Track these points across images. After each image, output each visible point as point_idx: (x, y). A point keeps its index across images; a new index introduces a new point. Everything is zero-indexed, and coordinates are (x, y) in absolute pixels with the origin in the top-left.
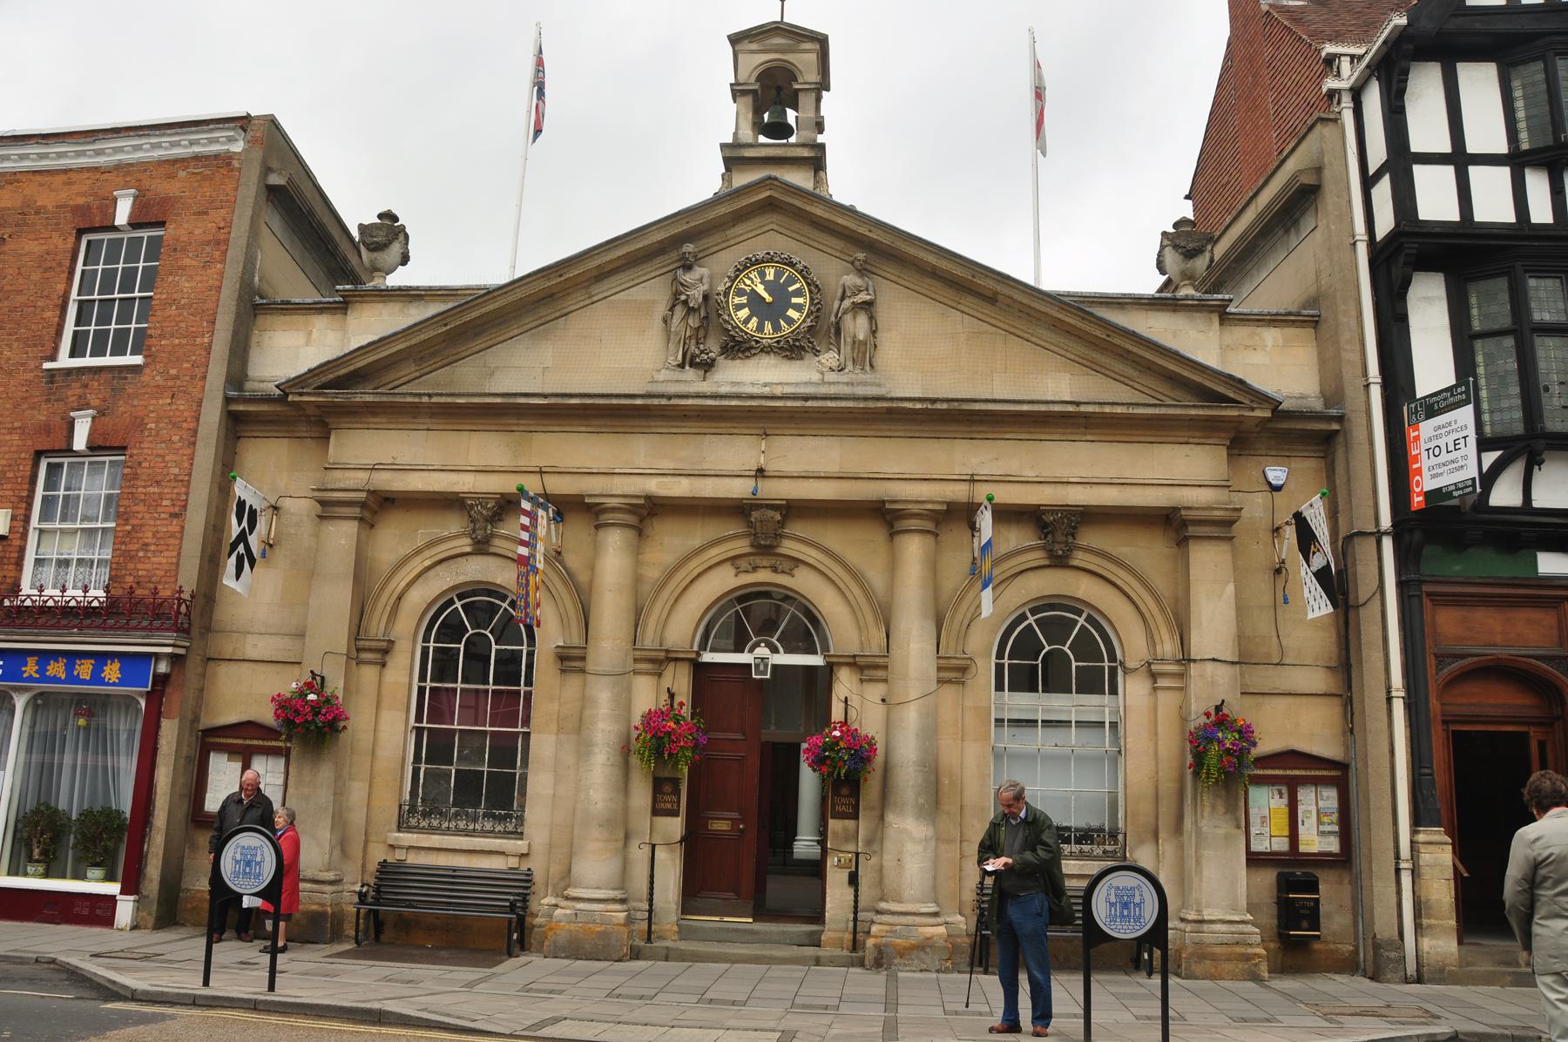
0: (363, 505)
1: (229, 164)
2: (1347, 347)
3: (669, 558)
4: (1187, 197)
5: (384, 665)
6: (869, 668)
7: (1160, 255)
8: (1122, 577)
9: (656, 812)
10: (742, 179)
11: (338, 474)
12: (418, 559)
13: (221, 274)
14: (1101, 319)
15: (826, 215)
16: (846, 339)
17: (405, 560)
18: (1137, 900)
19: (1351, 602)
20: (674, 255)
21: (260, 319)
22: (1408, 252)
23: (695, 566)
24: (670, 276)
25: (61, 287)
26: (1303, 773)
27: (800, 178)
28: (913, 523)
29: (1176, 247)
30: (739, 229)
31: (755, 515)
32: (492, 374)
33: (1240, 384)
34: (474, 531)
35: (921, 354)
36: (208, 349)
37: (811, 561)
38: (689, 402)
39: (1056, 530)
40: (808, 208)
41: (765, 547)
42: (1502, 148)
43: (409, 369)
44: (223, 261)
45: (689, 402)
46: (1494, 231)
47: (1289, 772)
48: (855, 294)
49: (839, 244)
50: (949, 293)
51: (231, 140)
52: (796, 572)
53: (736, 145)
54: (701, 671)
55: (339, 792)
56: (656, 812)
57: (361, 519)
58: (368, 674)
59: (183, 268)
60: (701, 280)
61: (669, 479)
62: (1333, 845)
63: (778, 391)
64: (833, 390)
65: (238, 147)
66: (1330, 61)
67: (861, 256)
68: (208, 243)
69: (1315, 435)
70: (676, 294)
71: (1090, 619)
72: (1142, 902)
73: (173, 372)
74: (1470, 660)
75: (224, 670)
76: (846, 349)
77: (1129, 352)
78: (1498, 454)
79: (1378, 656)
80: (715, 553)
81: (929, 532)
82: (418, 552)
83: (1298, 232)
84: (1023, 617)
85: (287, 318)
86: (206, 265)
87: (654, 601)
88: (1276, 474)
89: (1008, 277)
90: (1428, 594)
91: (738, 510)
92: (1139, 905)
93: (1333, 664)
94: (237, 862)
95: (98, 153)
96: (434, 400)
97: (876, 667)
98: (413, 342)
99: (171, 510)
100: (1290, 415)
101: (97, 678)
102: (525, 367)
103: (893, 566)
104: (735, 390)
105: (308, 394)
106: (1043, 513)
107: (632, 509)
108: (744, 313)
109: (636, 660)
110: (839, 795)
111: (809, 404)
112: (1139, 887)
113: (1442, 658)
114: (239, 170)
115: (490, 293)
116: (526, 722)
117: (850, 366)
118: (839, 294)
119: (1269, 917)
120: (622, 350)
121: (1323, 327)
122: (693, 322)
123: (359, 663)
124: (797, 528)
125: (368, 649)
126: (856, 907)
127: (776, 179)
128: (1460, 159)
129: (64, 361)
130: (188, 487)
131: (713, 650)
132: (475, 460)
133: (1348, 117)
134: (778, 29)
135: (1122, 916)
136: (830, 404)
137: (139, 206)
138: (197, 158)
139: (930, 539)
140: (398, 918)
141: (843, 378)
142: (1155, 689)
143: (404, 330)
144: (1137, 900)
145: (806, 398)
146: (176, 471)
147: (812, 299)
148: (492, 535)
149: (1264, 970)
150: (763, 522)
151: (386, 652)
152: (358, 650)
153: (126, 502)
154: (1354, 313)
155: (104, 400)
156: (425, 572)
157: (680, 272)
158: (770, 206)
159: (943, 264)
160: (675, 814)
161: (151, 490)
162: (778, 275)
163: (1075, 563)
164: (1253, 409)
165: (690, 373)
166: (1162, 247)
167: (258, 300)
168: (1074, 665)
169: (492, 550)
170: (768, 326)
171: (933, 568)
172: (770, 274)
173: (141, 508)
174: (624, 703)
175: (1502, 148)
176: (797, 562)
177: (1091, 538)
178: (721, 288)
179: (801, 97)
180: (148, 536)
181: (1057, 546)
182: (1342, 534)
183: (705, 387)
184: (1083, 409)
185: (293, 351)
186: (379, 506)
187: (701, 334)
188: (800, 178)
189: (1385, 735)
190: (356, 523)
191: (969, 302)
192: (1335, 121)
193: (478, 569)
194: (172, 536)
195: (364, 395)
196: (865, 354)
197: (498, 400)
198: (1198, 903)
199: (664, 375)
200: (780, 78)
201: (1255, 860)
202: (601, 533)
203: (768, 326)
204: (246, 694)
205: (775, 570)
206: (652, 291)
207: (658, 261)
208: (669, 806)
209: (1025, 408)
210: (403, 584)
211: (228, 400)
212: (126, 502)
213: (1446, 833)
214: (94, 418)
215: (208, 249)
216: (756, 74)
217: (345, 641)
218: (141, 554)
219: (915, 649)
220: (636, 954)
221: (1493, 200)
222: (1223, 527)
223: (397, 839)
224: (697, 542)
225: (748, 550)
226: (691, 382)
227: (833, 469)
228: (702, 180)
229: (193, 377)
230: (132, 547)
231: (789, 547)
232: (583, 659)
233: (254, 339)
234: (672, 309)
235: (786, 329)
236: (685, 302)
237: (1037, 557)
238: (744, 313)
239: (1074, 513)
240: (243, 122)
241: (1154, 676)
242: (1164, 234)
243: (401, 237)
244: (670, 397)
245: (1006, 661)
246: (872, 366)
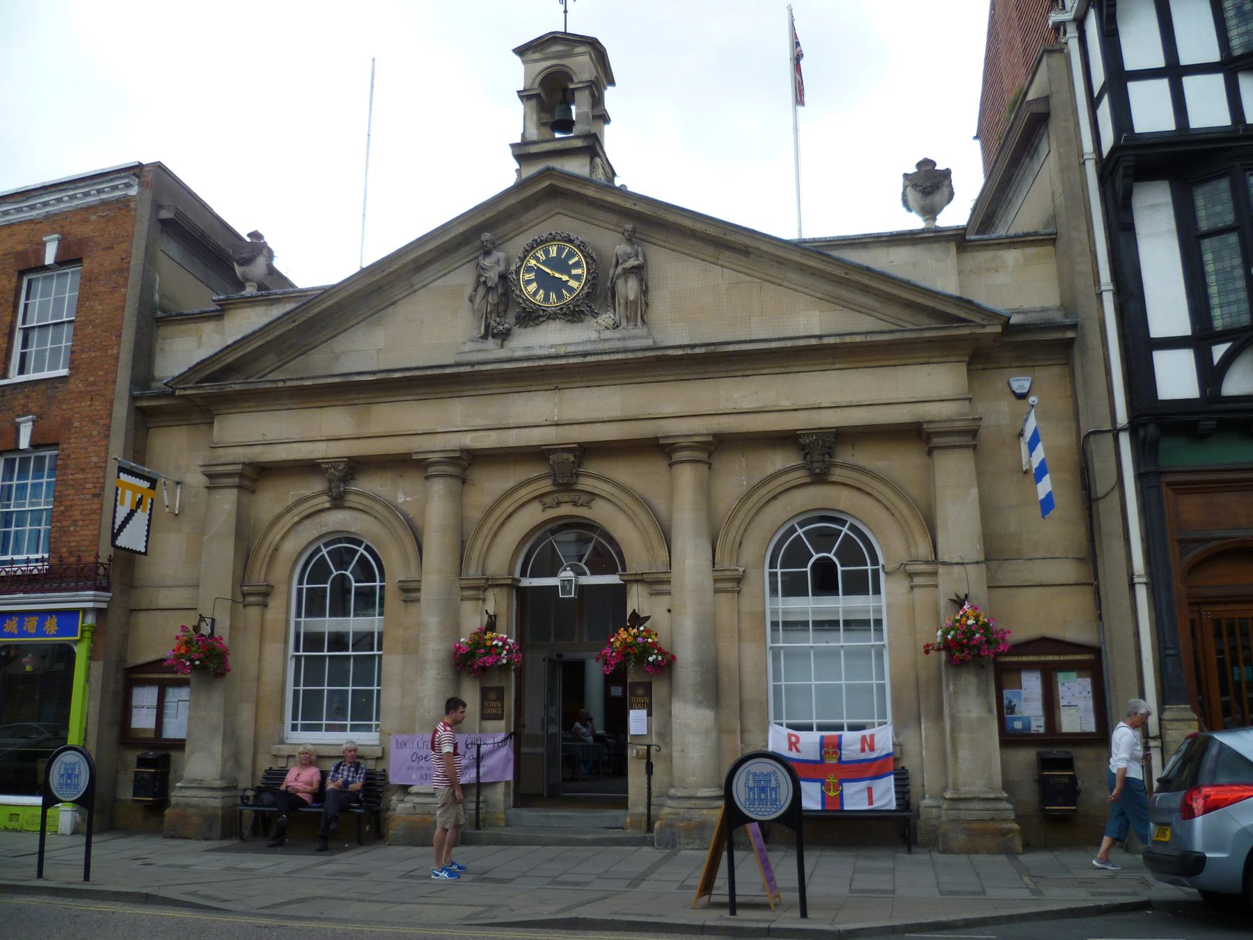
0: (241, 475)
1: (128, 206)
3: (488, 500)
4: (976, 138)
5: (265, 606)
6: (658, 583)
7: (904, 195)
9: (485, 717)
11: (221, 451)
12: (289, 516)
13: (124, 296)
14: (838, 260)
16: (620, 299)
17: (278, 518)
18: (773, 784)
19: (1093, 497)
20: (477, 243)
22: (1137, 162)
23: (508, 506)
24: (473, 264)
25: (8, 319)
26: (1056, 658)
27: (577, 166)
28: (685, 455)
29: (915, 186)
30: (530, 215)
31: (553, 458)
34: (330, 489)
35: (690, 308)
36: (116, 358)
37: (604, 494)
38: (489, 367)
39: (819, 450)
41: (565, 484)
42: (1214, 55)
43: (271, 360)
44: (126, 286)
46: (1211, 137)
47: (1043, 658)
48: (625, 261)
49: (614, 218)
50: (710, 250)
51: (128, 186)
52: (593, 504)
53: (525, 143)
55: (230, 715)
56: (485, 717)
57: (239, 487)
58: (254, 612)
59: (96, 294)
60: (498, 262)
61: (482, 433)
62: (1090, 726)
63: (562, 351)
64: (607, 346)
65: (133, 192)
67: (629, 226)
68: (114, 272)
69: (1045, 343)
70: (479, 276)
71: (853, 528)
72: (778, 786)
73: (91, 379)
74: (1214, 544)
75: (142, 616)
76: (620, 309)
78: (1228, 345)
79: (1119, 545)
80: (524, 493)
82: (288, 510)
85: (183, 327)
86: (114, 290)
87: (476, 536)
89: (754, 232)
90: (1168, 484)
91: (536, 454)
93: (1083, 555)
94: (62, 776)
95: (32, 207)
96: (288, 384)
97: (662, 582)
99: (93, 491)
100: (1022, 328)
101: (40, 632)
102: (365, 350)
103: (671, 495)
104: (527, 353)
107: (451, 461)
109: (463, 588)
110: (635, 695)
111: (588, 359)
112: (774, 773)
113: (1185, 543)
114: (135, 209)
117: (624, 323)
118: (614, 262)
120: (438, 329)
121: (1059, 243)
122: (492, 299)
124: (591, 467)
125: (251, 592)
127: (553, 169)
128: (1174, 71)
129: (15, 378)
130: (105, 472)
131: (532, 576)
132: (327, 431)
133: (1074, 46)
135: (761, 799)
136: (550, 362)
137: (63, 247)
138: (104, 203)
140: (278, 817)
142: (912, 588)
143: (261, 329)
144: (773, 784)
145: (585, 355)
146: (95, 459)
148: (346, 492)
149: (1018, 843)
150: (566, 464)
151: (266, 594)
152: (244, 595)
153: (60, 488)
154: (1085, 228)
155: (41, 407)
156: (297, 527)
157: (481, 258)
158: (553, 193)
159: (698, 226)
161: (78, 476)
162: (560, 251)
163: (834, 479)
164: (983, 326)
165: (491, 343)
166: (905, 188)
167: (159, 314)
169: (347, 504)
170: (553, 296)
171: (706, 493)
172: (553, 252)
173: (71, 492)
175: (1214, 55)
176: (593, 496)
177: (846, 455)
178: (513, 268)
179: (577, 94)
180: (76, 514)
181: (816, 465)
182: (1083, 433)
183: (503, 353)
185: (183, 352)
186: (258, 474)
187: (501, 308)
188: (577, 166)
189: (1129, 619)
190: (235, 491)
192: (1061, 51)
193: (337, 520)
194: (95, 513)
195: (235, 385)
196: (639, 311)
200: (565, 84)
201: (1010, 739)
202: (676, 467)
203: (553, 296)
204: (158, 638)
205: (575, 504)
206: (462, 278)
209: (774, 345)
210: (278, 537)
211: (133, 399)
212: (60, 488)
213: (1193, 709)
214: (34, 422)
215: (114, 276)
216: (539, 79)
218: (72, 529)
219: (691, 562)
221: (1208, 106)
222: (969, 436)
224: (510, 484)
226: (492, 350)
227: (617, 414)
228: (502, 174)
229: (106, 382)
230: (66, 523)
231: (586, 484)
232: (418, 590)
234: (475, 290)
235: (568, 297)
236: (485, 283)
237: (799, 476)
238: (533, 287)
240: (136, 170)
241: (911, 575)
242: (906, 175)
243: (265, 252)
244: (473, 364)
245: (779, 571)
246: (643, 321)
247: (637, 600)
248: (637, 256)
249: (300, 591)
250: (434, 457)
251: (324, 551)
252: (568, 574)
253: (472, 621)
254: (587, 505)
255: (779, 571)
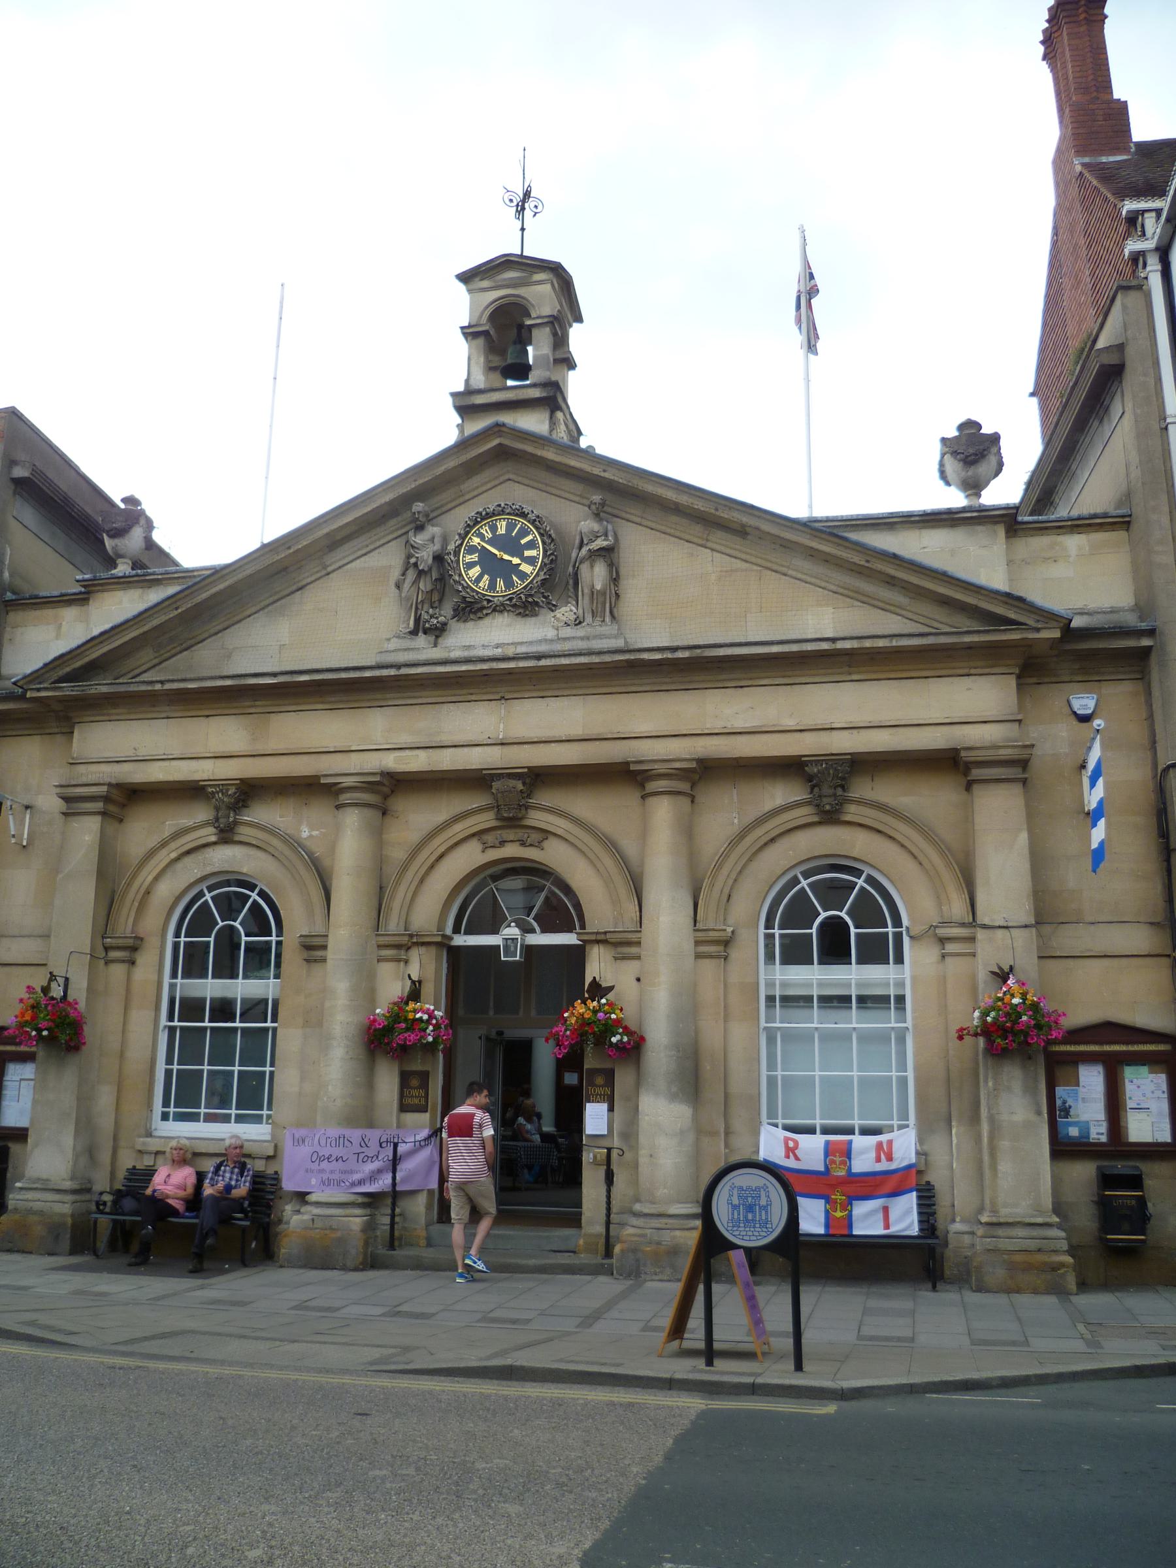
0: (106, 799)
2: (1159, 548)
3: (414, 837)
5: (133, 963)
6: (624, 945)
8: (902, 830)
9: (404, 1108)
10: (477, 425)
11: (82, 768)
12: (164, 852)
14: (857, 543)
15: (558, 458)
17: (151, 854)
18: (763, 1202)
21: (12, 615)
23: (439, 844)
24: (403, 540)
26: (1123, 1048)
27: (533, 422)
29: (955, 453)
30: (475, 481)
31: (496, 785)
32: (229, 657)
33: (1018, 601)
34: (217, 819)
35: (671, 596)
38: (420, 670)
39: (829, 782)
40: (539, 453)
41: (511, 819)
43: (146, 656)
45: (420, 670)
47: (1107, 1048)
49: (578, 488)
50: (698, 529)
52: (546, 844)
53: (469, 392)
54: (455, 955)
55: (84, 1101)
56: (404, 1108)
57: (103, 814)
60: (432, 540)
61: (408, 753)
63: (510, 651)
64: (567, 646)
66: (1133, 220)
67: (597, 498)
70: (409, 556)
72: (769, 1204)
76: (584, 601)
77: (893, 577)
80: (460, 829)
81: (679, 793)
82: (164, 844)
83: (1110, 421)
84: (795, 881)
85: (38, 613)
87: (398, 882)
88: (1084, 703)
92: (765, 1208)
96: (167, 686)
97: (629, 944)
98: (146, 628)
102: (266, 646)
103: (644, 834)
104: (466, 654)
105: (46, 689)
106: (806, 764)
108: (475, 571)
111: (543, 662)
112: (765, 1187)
115: (218, 573)
116: (275, 1019)
117: (589, 619)
118: (577, 542)
119: (1086, 1219)
120: (353, 621)
121: (1134, 527)
122: (425, 585)
123: (107, 963)
124: (546, 797)
125: (115, 946)
126: (609, 1209)
127: (504, 425)
134: (505, 263)
139: (686, 801)
140: (139, 1229)
141: (580, 632)
143: (135, 617)
144: (763, 1202)
145: (539, 657)
147: (545, 551)
148: (236, 823)
149: (1071, 1281)
150: (513, 793)
151: (134, 949)
156: (175, 865)
158: (503, 454)
159: (684, 499)
160: (423, 1109)
162: (510, 527)
163: (848, 818)
164: (1038, 630)
165: (422, 640)
166: (943, 455)
168: (853, 931)
169: (237, 838)
170: (500, 583)
171: (688, 832)
174: (367, 991)
176: (546, 833)
177: (863, 788)
178: (451, 547)
181: (825, 800)
184: (840, 645)
186: (127, 798)
187: (436, 597)
188: (533, 422)
190: (98, 818)
191: (718, 536)
192: (1139, 287)
193: (225, 858)
195: (101, 686)
196: (608, 603)
197: (229, 682)
198: (993, 1203)
199: (394, 644)
201: (1063, 1149)
203: (500, 583)
205: (523, 844)
207: (392, 522)
208: (416, 1101)
209: (775, 649)
210: (150, 878)
217: (88, 941)
219: (667, 918)
220: (371, 1263)
223: (144, 1144)
224: (442, 817)
225: (494, 823)
226: (423, 649)
227: (577, 731)
231: (537, 818)
233: (7, 636)
235: (519, 584)
236: (416, 565)
237: (805, 814)
238: (475, 571)
239: (843, 761)
241: (943, 941)
245: (777, 932)
247: (598, 965)
248: (606, 535)
249: (176, 946)
250: (348, 781)
251: (208, 897)
252: (512, 931)
253: (391, 988)
254: (538, 845)
255: (777, 932)
